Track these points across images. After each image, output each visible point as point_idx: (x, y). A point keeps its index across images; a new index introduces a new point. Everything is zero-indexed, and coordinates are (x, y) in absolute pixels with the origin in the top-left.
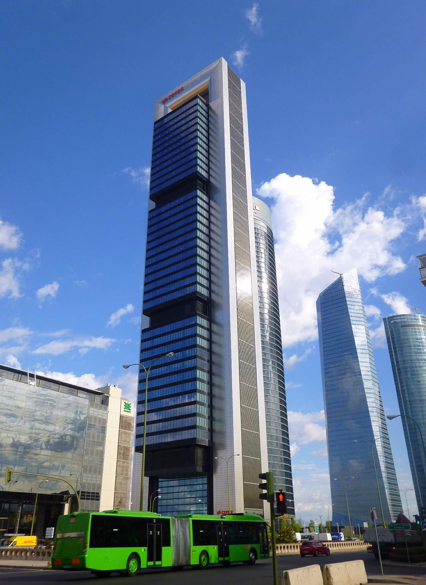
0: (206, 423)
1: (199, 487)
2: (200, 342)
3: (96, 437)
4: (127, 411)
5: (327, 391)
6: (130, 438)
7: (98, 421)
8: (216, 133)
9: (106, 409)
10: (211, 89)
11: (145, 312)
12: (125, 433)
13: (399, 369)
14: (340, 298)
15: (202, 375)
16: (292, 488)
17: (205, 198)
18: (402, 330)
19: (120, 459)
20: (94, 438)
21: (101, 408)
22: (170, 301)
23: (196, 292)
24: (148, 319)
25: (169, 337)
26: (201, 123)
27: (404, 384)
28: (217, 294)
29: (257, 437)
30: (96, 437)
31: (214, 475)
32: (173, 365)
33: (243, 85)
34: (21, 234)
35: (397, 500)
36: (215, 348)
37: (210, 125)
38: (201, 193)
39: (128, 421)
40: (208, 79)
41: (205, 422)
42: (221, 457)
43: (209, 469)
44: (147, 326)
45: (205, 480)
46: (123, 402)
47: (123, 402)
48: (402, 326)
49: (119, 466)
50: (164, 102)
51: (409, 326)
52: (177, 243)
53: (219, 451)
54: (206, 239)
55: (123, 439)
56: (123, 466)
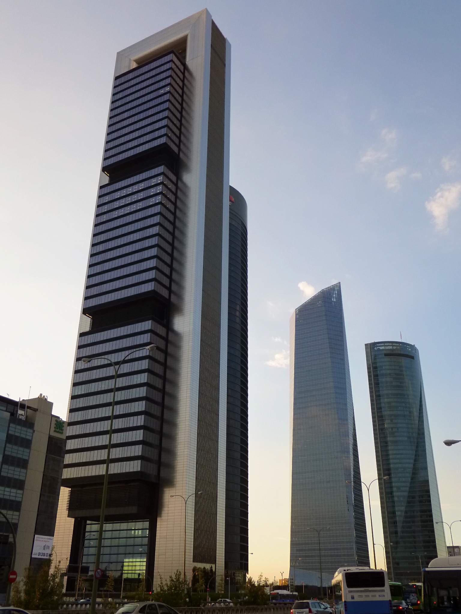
4: (58, 432)
8: (191, 84)
34: (256, 584)
44: (87, 329)
45: (147, 524)
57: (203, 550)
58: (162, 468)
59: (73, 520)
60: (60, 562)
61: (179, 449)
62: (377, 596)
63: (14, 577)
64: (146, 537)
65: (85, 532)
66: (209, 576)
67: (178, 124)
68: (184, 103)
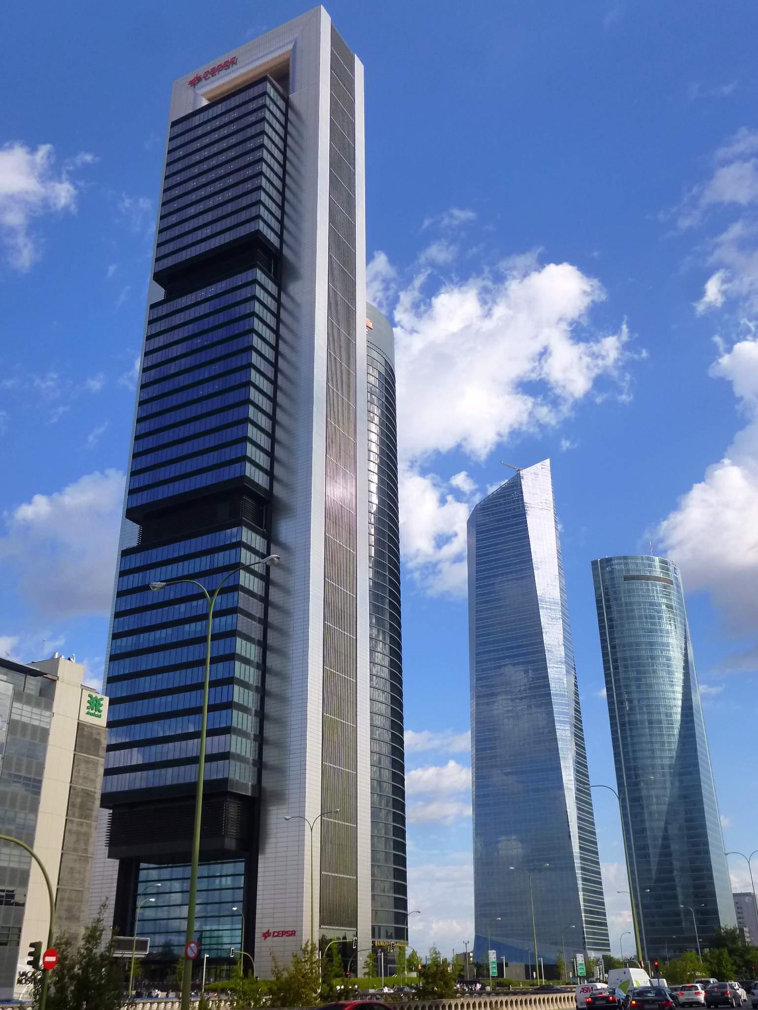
0: (248, 749)
1: (228, 882)
2: (245, 579)
3: (24, 767)
5: (478, 697)
6: (96, 772)
7: (29, 733)
9: (49, 706)
10: (294, 67)
11: (131, 514)
12: (87, 761)
13: (615, 661)
14: (514, 517)
15: (246, 648)
16: (405, 887)
17: (272, 287)
18: (624, 586)
19: (74, 816)
20: (18, 770)
21: (38, 705)
22: (185, 494)
23: (243, 478)
24: (135, 528)
25: (186, 567)
26: (272, 131)
27: (623, 690)
28: (285, 485)
29: (353, 780)
30: (24, 767)
31: (260, 857)
32: (187, 627)
33: (359, 68)
35: (598, 913)
36: (275, 595)
37: (289, 141)
38: (263, 276)
39: (95, 736)
40: (290, 47)
41: (249, 746)
42: (276, 819)
43: (249, 846)
44: (134, 542)
45: (241, 867)
46: (86, 693)
47: (86, 693)
48: (626, 578)
49: (70, 831)
50: (194, 83)
51: (638, 578)
52: (207, 376)
53: (275, 808)
54: (270, 373)
55: (81, 774)
56: (78, 833)
57: (339, 910)
58: (264, 772)
59: (116, 862)
60: (107, 898)
61: (291, 773)
62: (339, 491)
63: (89, 812)
64: (240, 888)
65: (137, 882)
66: (348, 951)
67: (278, 213)
68: (287, 177)
